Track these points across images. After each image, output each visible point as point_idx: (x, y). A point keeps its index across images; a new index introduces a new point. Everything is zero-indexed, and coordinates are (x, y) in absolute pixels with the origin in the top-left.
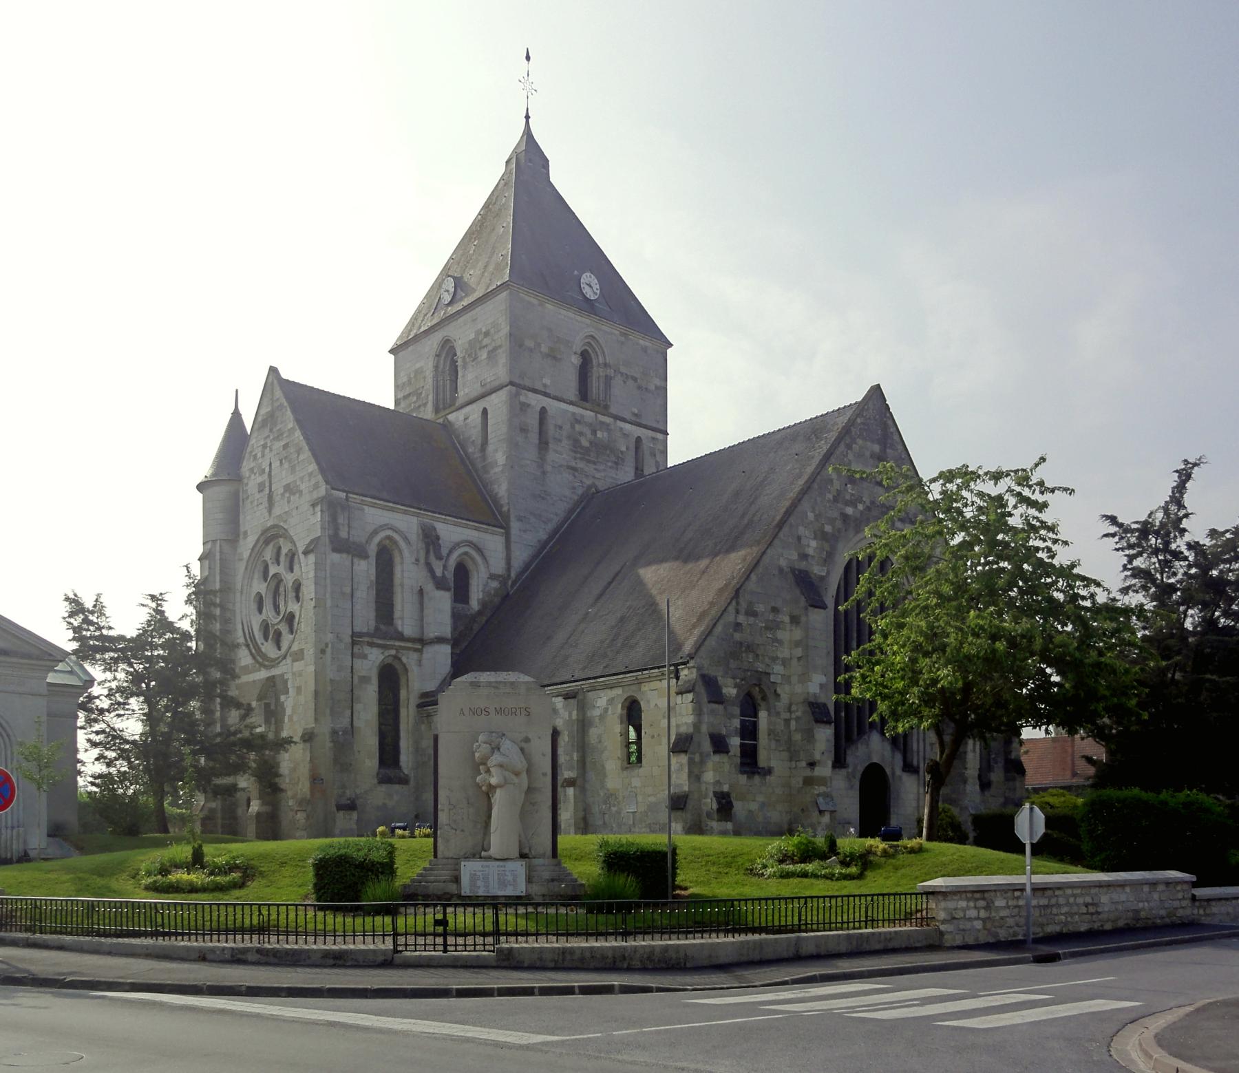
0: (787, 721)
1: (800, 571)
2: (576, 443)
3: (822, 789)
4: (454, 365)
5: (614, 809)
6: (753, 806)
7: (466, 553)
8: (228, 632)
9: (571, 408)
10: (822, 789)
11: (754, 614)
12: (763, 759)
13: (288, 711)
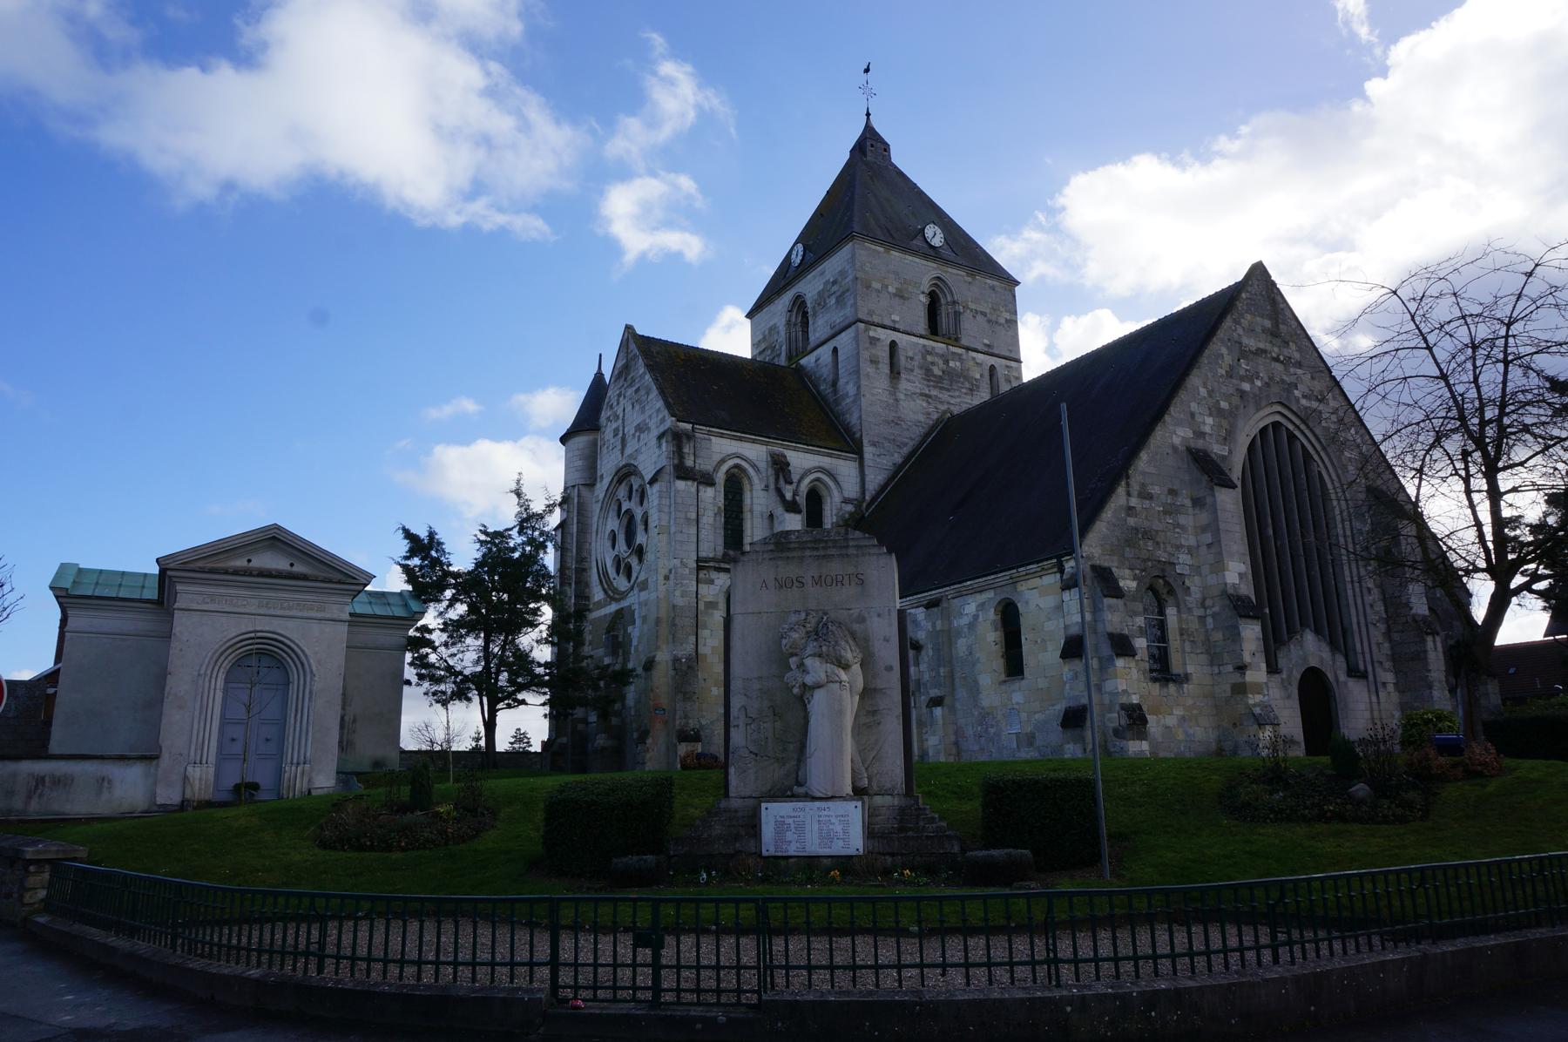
0: (1202, 619)
1: (1198, 451)
2: (928, 372)
3: (1258, 698)
4: (805, 315)
5: (992, 731)
6: (1171, 721)
7: (818, 479)
8: (584, 570)
9: (922, 341)
10: (1258, 698)
11: (1150, 497)
12: (1176, 667)
13: (635, 642)
